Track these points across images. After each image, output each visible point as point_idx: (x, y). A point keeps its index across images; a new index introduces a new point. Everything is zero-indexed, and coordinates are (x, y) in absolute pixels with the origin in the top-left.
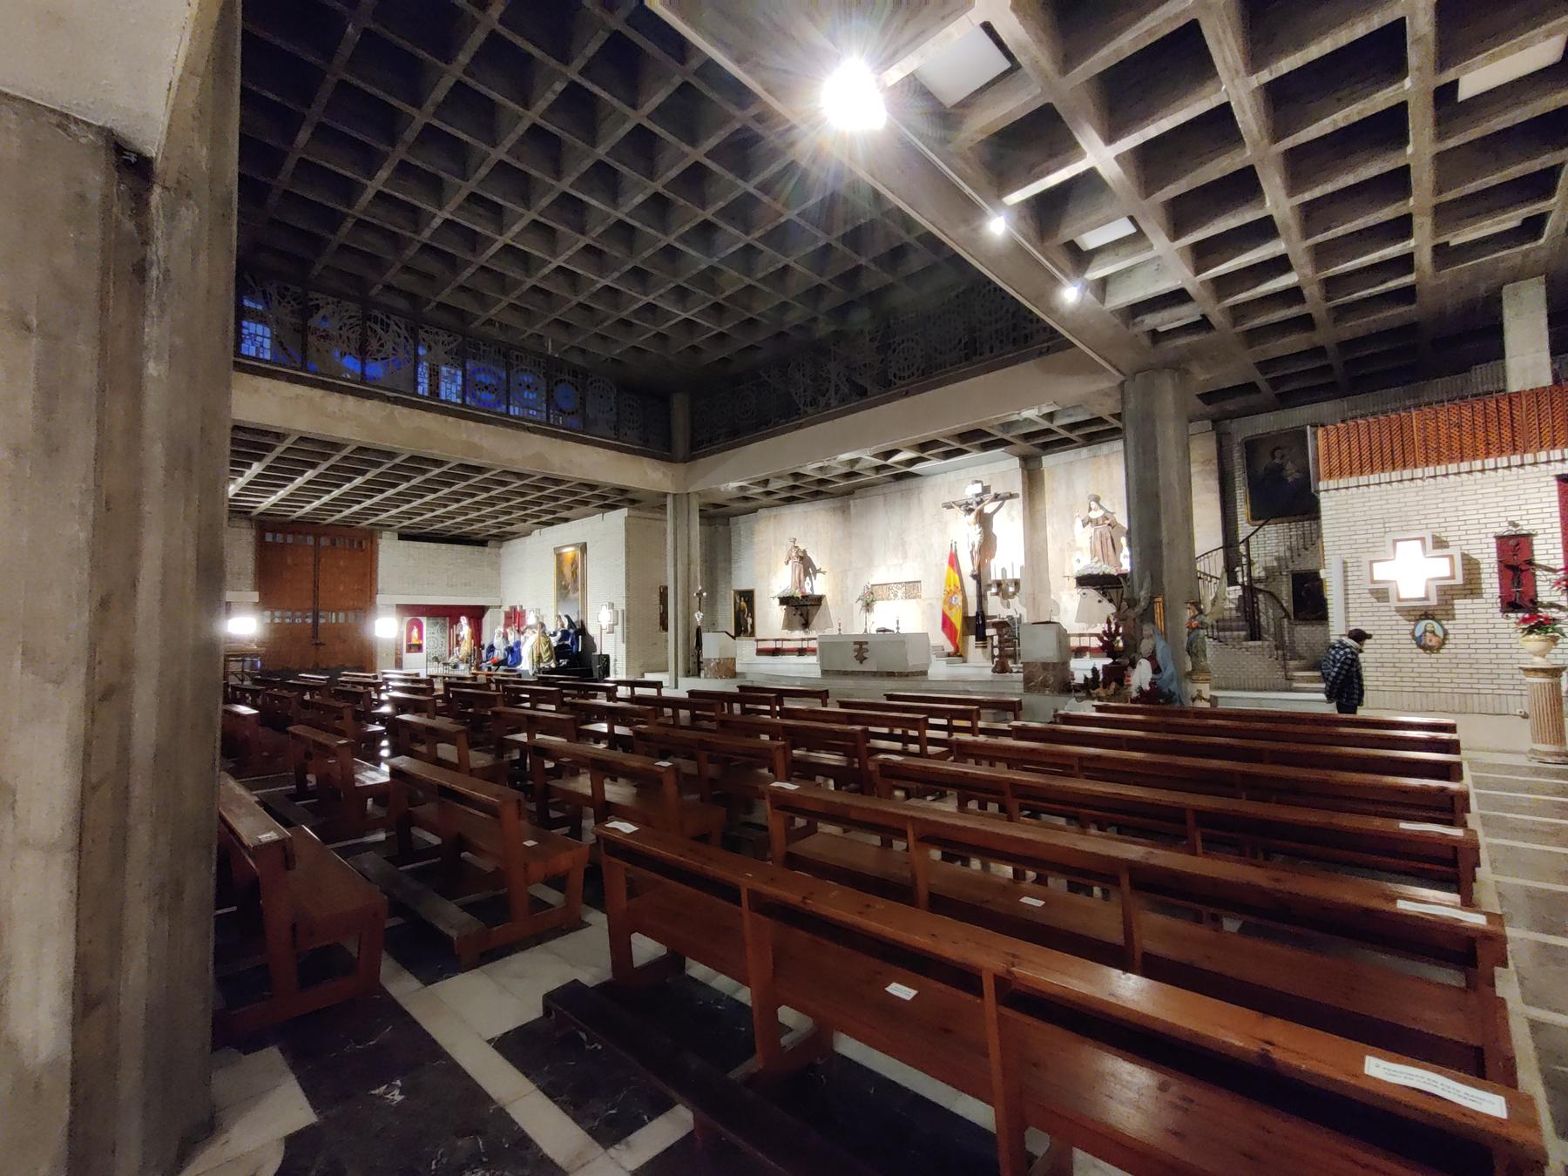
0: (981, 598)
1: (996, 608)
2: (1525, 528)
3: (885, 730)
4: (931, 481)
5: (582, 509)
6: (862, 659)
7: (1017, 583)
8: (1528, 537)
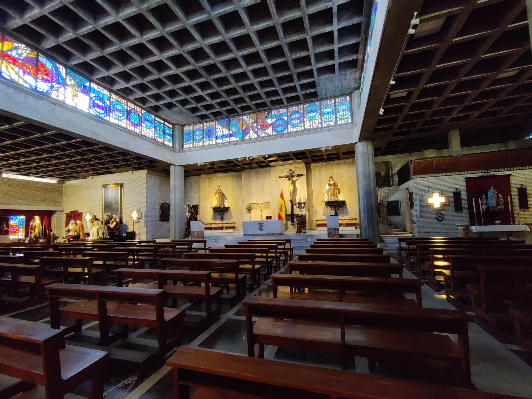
0: (292, 208)
1: (297, 211)
2: (525, 186)
3: (260, 254)
4: (273, 168)
5: (125, 168)
6: (261, 230)
7: (304, 203)
8: (460, 192)
